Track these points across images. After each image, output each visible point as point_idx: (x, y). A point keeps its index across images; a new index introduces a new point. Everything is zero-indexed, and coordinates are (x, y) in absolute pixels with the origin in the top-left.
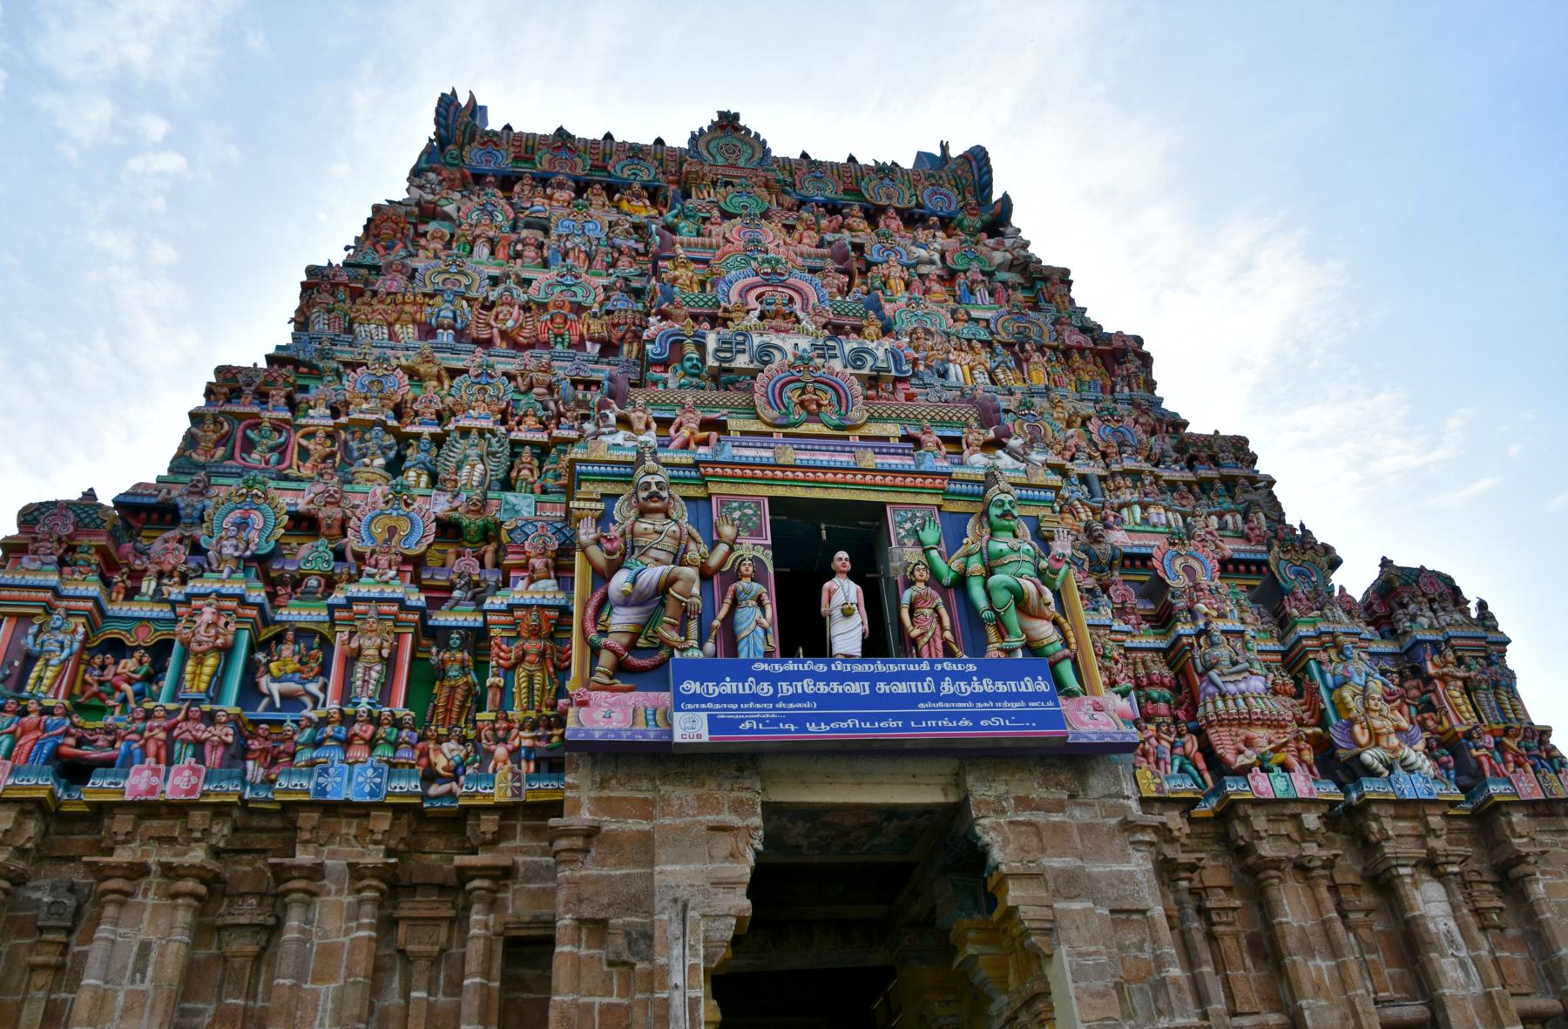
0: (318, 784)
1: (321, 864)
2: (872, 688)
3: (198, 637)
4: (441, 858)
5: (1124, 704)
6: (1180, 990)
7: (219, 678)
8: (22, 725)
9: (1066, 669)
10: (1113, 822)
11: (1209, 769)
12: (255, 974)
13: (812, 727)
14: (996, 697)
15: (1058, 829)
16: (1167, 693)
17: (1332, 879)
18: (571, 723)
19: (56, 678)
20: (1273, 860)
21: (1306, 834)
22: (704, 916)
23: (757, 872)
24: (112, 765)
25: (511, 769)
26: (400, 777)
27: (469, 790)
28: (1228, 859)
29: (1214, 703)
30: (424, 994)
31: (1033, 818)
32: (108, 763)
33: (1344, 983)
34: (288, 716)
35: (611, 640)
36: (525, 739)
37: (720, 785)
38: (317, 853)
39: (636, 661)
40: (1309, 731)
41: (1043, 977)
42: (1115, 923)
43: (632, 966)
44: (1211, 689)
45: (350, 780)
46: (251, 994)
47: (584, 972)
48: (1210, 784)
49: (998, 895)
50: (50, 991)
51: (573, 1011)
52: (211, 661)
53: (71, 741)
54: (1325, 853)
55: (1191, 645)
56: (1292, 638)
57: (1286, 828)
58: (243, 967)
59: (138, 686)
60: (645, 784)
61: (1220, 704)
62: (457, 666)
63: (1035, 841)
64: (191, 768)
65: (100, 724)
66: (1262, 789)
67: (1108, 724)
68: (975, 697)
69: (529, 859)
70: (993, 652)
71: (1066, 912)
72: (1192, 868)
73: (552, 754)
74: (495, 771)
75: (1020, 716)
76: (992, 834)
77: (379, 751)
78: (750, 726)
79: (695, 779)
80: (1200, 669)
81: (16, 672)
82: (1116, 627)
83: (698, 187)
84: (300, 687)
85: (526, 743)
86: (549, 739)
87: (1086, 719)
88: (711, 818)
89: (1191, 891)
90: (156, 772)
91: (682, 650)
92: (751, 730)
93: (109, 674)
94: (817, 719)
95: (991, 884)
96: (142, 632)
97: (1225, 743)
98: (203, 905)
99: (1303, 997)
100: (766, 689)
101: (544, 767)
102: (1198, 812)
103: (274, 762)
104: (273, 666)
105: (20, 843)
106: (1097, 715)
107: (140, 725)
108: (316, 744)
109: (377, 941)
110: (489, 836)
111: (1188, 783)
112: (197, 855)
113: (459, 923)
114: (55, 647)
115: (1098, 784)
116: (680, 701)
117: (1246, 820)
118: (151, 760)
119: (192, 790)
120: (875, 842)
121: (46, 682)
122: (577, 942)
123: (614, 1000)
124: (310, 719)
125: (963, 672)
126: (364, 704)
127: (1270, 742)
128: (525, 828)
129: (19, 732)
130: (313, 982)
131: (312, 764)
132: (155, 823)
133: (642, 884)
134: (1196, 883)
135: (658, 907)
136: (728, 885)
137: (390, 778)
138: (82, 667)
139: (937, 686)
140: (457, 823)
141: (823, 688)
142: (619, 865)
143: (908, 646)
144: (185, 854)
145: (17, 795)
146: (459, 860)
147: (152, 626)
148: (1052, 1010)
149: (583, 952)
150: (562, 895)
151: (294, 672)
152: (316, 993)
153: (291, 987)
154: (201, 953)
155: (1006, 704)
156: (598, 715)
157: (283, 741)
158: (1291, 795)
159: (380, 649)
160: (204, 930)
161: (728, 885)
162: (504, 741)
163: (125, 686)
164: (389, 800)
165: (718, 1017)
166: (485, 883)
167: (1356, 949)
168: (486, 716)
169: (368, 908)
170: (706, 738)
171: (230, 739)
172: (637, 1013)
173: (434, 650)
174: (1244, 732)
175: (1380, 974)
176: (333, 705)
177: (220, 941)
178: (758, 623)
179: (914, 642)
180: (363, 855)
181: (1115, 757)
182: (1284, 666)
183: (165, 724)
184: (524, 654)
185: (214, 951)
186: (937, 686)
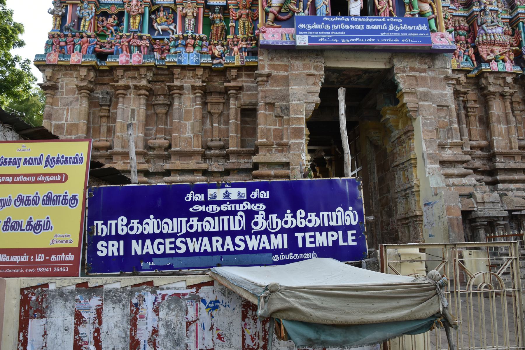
0: (179, 60)
1: (183, 85)
2: (365, 27)
3: (133, 10)
4: (218, 84)
5: (450, 36)
6: (456, 131)
7: (141, 24)
8: (82, 41)
9: (432, 22)
10: (442, 76)
11: (476, 60)
12: (166, 118)
13: (343, 41)
14: (408, 31)
15: (424, 78)
16: (465, 33)
17: (511, 100)
18: (261, 39)
19: (89, 25)
20: (493, 92)
21: (506, 84)
22: (305, 103)
23: (322, 89)
24: (113, 54)
25: (240, 55)
26: (204, 57)
27: (226, 62)
28: (477, 91)
29: (482, 36)
30: (217, 125)
31: (415, 74)
32: (112, 53)
33: (509, 132)
34: (165, 37)
35: (273, 9)
36: (244, 45)
37: (310, 61)
38: (181, 82)
39: (281, 17)
40: (514, 48)
41: (412, 125)
42: (438, 110)
43: (282, 117)
44: (482, 32)
45: (189, 58)
46: (166, 124)
47: (268, 119)
48: (476, 65)
49: (400, 100)
50: (107, 123)
51: (265, 130)
52: (138, 18)
53: (98, 46)
54: (511, 91)
55: (477, 15)
56: (516, 13)
57: (500, 82)
58: (162, 116)
59: (115, 28)
60: (285, 60)
61: (484, 37)
62: (218, 19)
63: (415, 82)
64: (138, 55)
65: (106, 41)
66: (494, 68)
67: (446, 42)
68: (401, 31)
69: (247, 84)
70: (407, 15)
71: (422, 105)
72: (465, 93)
73: (252, 50)
74: (234, 55)
75: (416, 38)
76: (400, 79)
77: (196, 49)
78: (323, 40)
79: (302, 58)
80: (479, 24)
81: (76, 24)
82: (451, 7)
84: (167, 27)
85: (244, 46)
86: (251, 44)
87: (438, 40)
88: (308, 72)
89: (463, 101)
90: (127, 56)
91: (298, 13)
92: (322, 42)
93: (105, 23)
94: (345, 38)
95: (398, 95)
96: (113, 9)
97: (483, 52)
98: (148, 98)
99: (494, 136)
100: (328, 27)
101: (250, 54)
102: (470, 75)
103: (163, 52)
104: (157, 19)
105: (90, 79)
106: (442, 39)
107: (119, 40)
108: (176, 47)
109: (202, 109)
110: (234, 77)
111: (469, 65)
112: (144, 82)
113: (226, 104)
114: (87, 14)
115: (438, 63)
116: (298, 31)
117: (486, 78)
118: (125, 52)
119: (139, 62)
120: (359, 81)
121: (86, 26)
122: (265, 110)
123: (277, 127)
124: (173, 38)
125: (397, 22)
126: (190, 33)
127: (500, 52)
128: (245, 74)
129: (82, 44)
130: (184, 121)
131: (176, 53)
132: (129, 72)
133: (285, 92)
134: (465, 99)
135: (291, 100)
136: (313, 93)
137: (201, 58)
138: (96, 22)
139: (388, 27)
140: (223, 72)
141: (347, 27)
142: (278, 86)
143: (376, 12)
144: (140, 82)
145: (86, 64)
146: (226, 84)
147: (116, 6)
148: (413, 135)
149: (267, 113)
150: (260, 95)
151: (165, 22)
152: (186, 124)
153: (178, 122)
154: (149, 112)
155: (411, 34)
156: (270, 36)
157: (165, 46)
158: (504, 70)
159: (193, 13)
160: (149, 105)
161: (313, 93)
162: (237, 45)
163: (111, 28)
164: (202, 65)
165: (309, 133)
166: (234, 92)
167: (515, 123)
168: (230, 37)
169: (198, 99)
170: (307, 44)
171: (148, 45)
172: (285, 131)
173: (210, 13)
174: (491, 48)
175: (521, 131)
176: (180, 33)
177: (154, 109)
178: (324, 3)
179: (379, 11)
180: (195, 82)
181: (446, 54)
182: (509, 24)
183: (127, 40)
184: (242, 15)
185: (153, 112)
186: (388, 27)
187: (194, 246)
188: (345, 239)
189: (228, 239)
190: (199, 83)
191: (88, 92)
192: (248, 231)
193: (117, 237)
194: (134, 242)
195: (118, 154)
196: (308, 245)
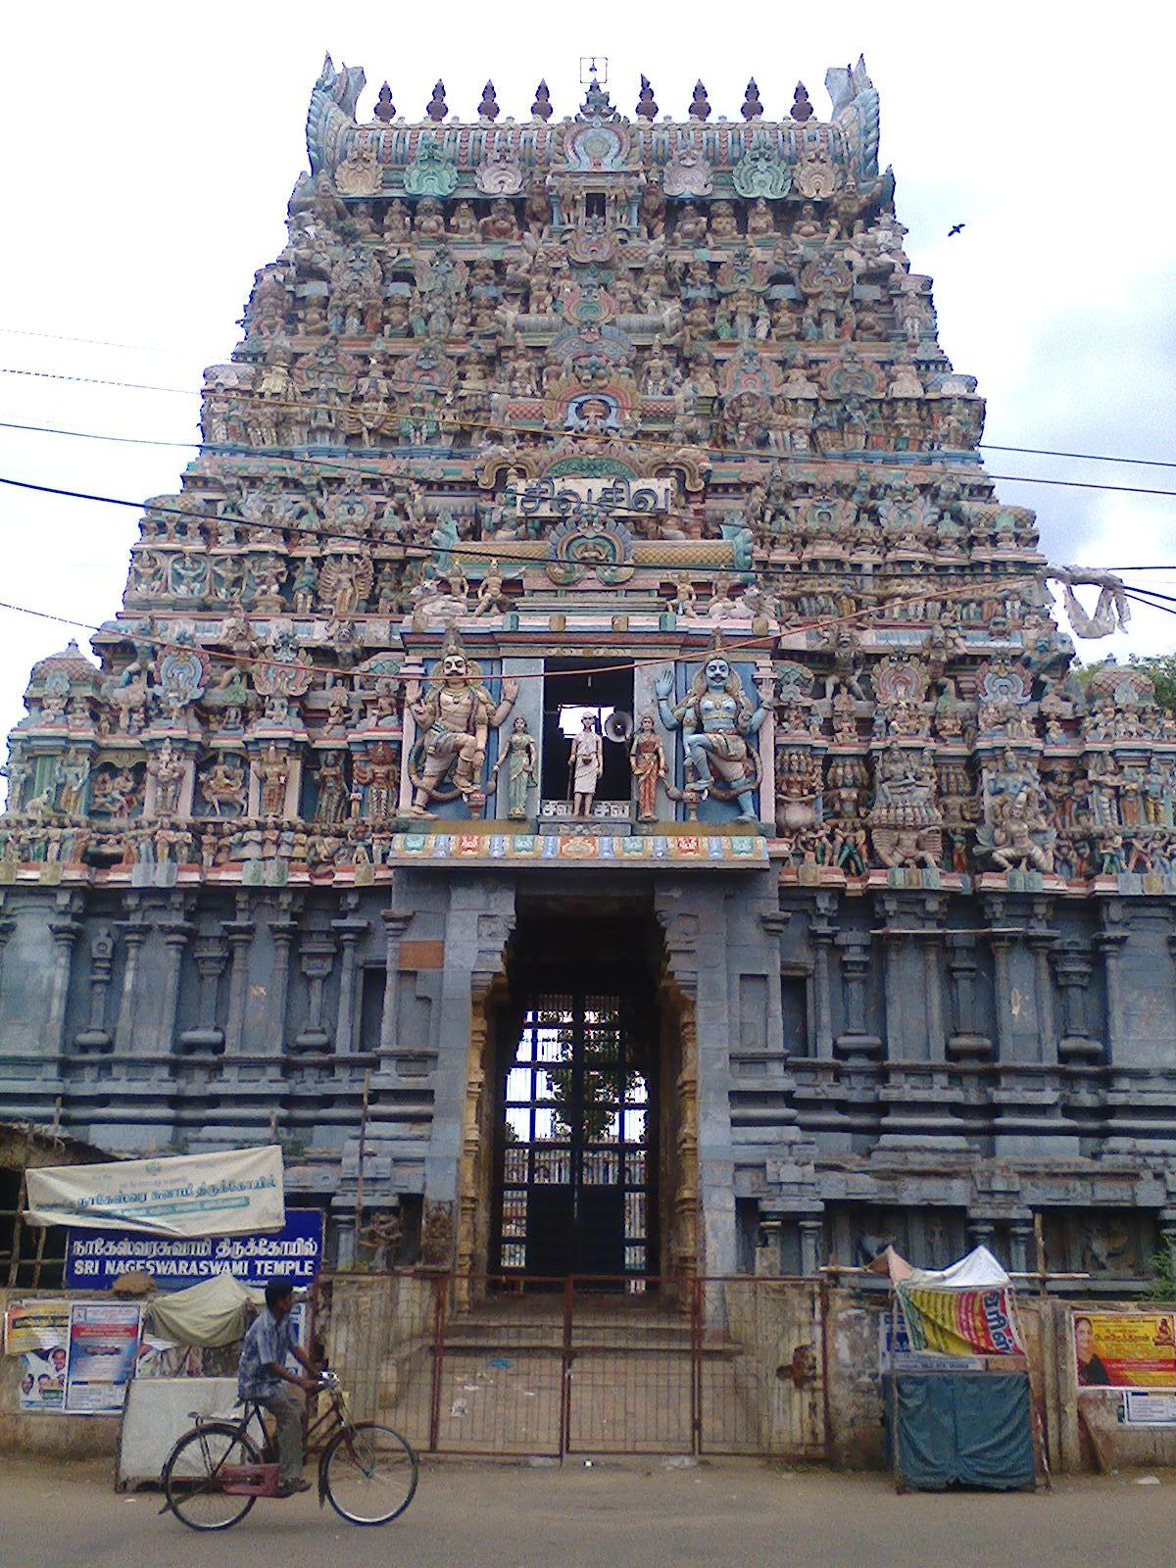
83: (559, 206)
113: (337, 957)
140: (334, 895)
146: (336, 923)
187: (162, 1269)
188: (302, 1268)
189: (194, 1264)
190: (285, 922)
191: (74, 941)
192: (212, 1257)
193: (93, 1258)
194: (108, 1263)
195: (120, 1062)
196: (266, 1272)
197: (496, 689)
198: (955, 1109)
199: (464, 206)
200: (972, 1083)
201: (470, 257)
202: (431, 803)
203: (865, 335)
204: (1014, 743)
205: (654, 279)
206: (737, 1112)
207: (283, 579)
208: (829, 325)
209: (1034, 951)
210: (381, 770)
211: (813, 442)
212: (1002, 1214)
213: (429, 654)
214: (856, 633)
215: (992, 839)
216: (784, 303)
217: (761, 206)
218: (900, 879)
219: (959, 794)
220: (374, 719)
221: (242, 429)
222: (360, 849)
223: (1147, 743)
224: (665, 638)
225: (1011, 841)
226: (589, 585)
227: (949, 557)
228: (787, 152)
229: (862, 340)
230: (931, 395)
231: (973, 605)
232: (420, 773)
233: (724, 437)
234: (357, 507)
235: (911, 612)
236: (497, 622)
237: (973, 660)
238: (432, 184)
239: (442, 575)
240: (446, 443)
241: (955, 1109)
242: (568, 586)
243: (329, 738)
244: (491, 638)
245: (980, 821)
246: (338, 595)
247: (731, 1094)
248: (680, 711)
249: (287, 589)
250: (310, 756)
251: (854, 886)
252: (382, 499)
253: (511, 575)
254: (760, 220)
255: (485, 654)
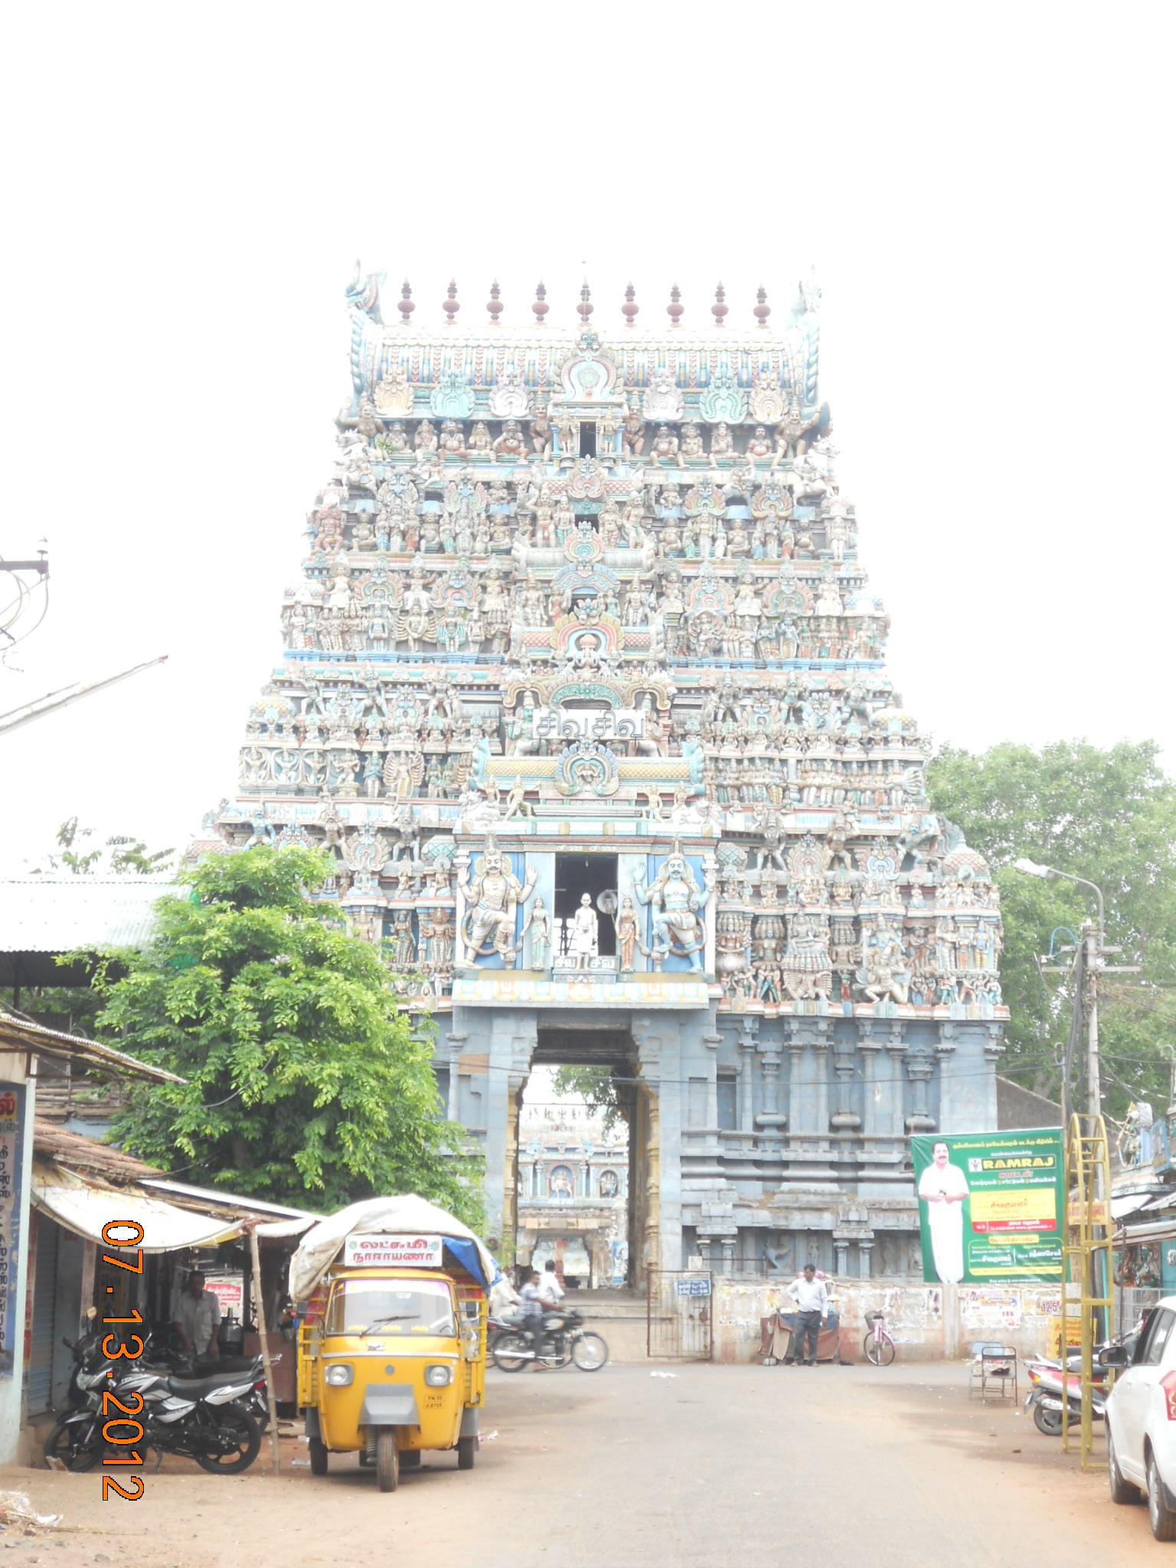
197: (521, 873)
198: (833, 1165)
199: (480, 426)
200: (846, 1148)
201: (486, 478)
202: (478, 957)
203: (802, 552)
204: (885, 911)
205: (635, 512)
206: (687, 1169)
207: (357, 769)
208: (773, 546)
209: (892, 1058)
210: (439, 929)
211: (757, 651)
212: (854, 1235)
213: (474, 848)
214: (781, 817)
215: (866, 979)
216: (738, 523)
217: (722, 430)
218: (801, 1008)
219: (847, 943)
220: (433, 890)
221: (316, 638)
222: (426, 984)
223: (977, 911)
224: (638, 839)
225: (879, 980)
226: (587, 796)
227: (853, 753)
228: (745, 378)
229: (799, 557)
230: (848, 613)
231: (868, 793)
232: (469, 935)
233: (688, 648)
234: (410, 711)
235: (823, 798)
236: (522, 827)
237: (866, 839)
238: (454, 407)
239: (481, 786)
240: (473, 651)
241: (833, 1165)
242: (572, 796)
243: (400, 900)
244: (518, 839)
245: (859, 963)
246: (399, 781)
247: (682, 1158)
248: (649, 893)
249: (359, 777)
250: (388, 915)
251: (770, 1011)
252: (425, 697)
253: (530, 788)
254: (723, 441)
255: (513, 848)
